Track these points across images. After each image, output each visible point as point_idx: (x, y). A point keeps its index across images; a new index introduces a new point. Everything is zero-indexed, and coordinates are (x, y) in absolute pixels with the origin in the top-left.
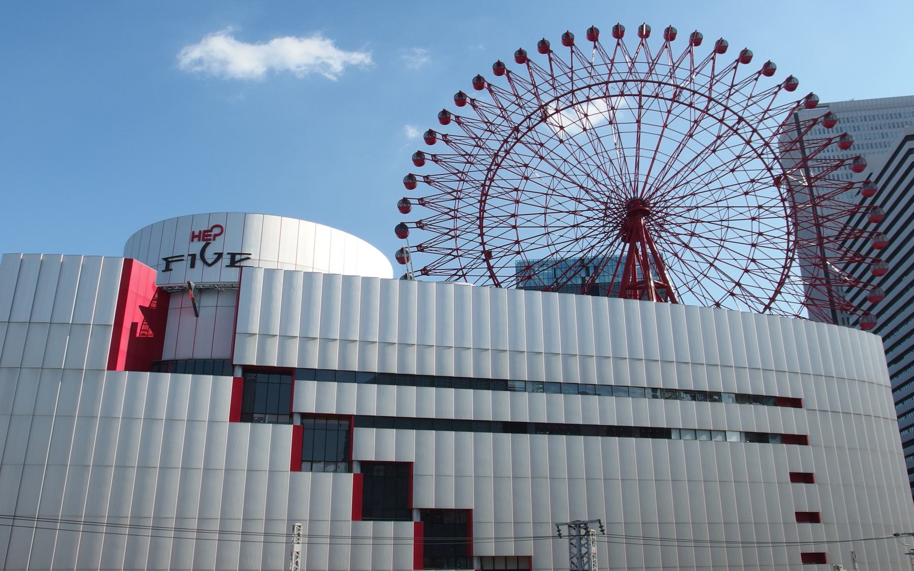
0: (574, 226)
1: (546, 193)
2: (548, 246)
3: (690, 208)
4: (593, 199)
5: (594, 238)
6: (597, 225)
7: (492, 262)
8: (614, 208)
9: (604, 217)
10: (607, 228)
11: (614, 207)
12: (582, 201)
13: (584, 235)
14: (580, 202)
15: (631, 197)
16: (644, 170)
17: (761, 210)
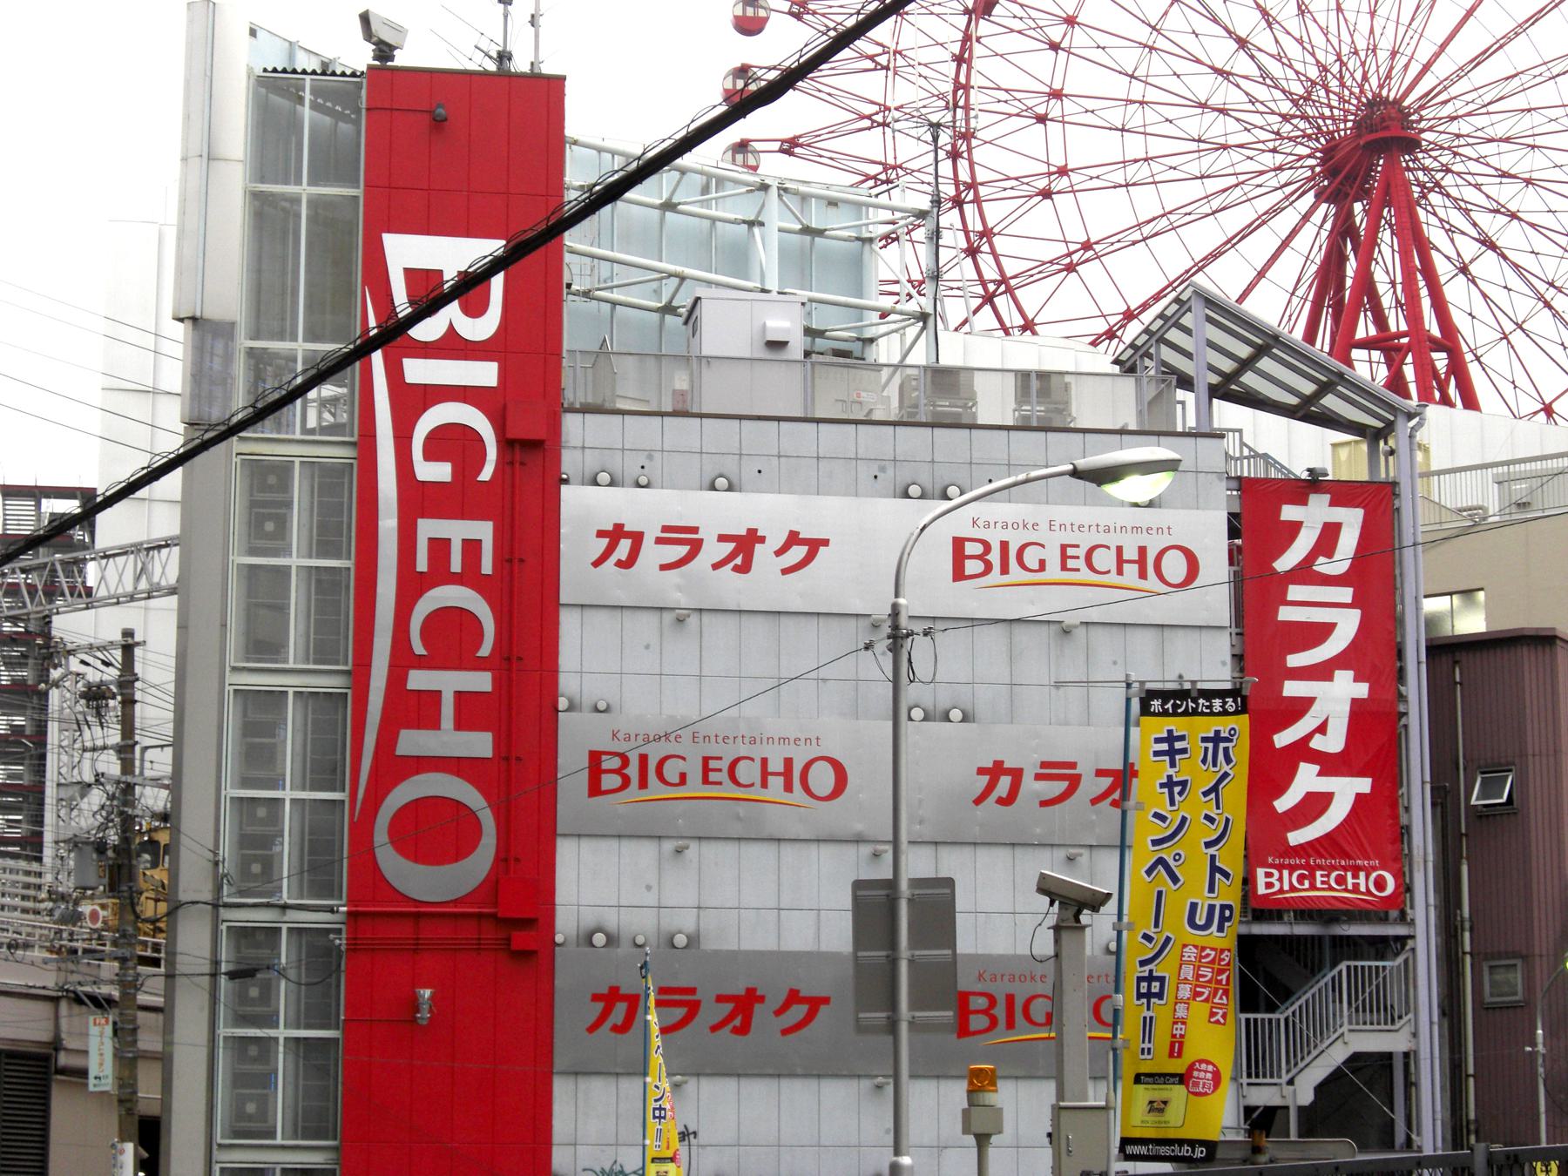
0: (1219, 72)
1: (1519, 330)
2: (1132, 76)
3: (1503, 210)
4: (1305, 38)
5: (1246, 129)
6: (1460, 181)
7: (984, 27)
8: (1335, 93)
9: (1431, 190)
10: (1444, 160)
11: (1337, 90)
12: (1276, 26)
13: (1226, 107)
14: (1270, 25)
15: (1388, 96)
16: (1463, 50)
17: (1041, 110)
